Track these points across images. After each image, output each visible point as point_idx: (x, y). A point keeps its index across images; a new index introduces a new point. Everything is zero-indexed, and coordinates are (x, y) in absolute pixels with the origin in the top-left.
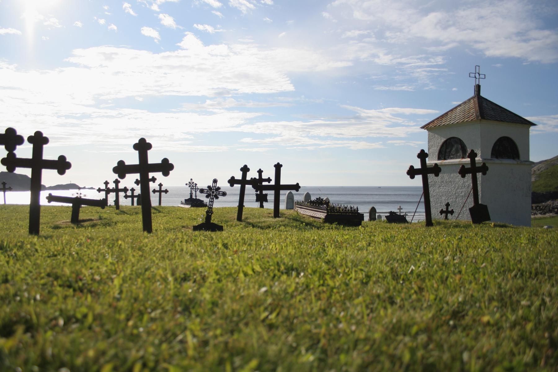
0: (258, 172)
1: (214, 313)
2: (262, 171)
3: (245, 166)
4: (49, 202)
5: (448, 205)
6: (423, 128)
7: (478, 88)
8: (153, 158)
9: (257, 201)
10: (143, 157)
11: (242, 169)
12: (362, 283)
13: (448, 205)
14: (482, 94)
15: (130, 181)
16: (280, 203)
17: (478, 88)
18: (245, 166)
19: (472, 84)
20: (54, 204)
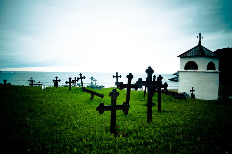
0: (114, 78)
1: (89, 131)
2: (120, 77)
3: (70, 78)
4: (154, 76)
5: (193, 88)
6: (178, 56)
7: (200, 42)
8: (83, 76)
9: (116, 85)
10: (81, 76)
11: (69, 79)
12: (141, 132)
13: (193, 88)
14: (202, 44)
15: (68, 84)
16: (216, 67)
17: (200, 42)
18: (70, 78)
19: (198, 40)
20: (153, 78)
